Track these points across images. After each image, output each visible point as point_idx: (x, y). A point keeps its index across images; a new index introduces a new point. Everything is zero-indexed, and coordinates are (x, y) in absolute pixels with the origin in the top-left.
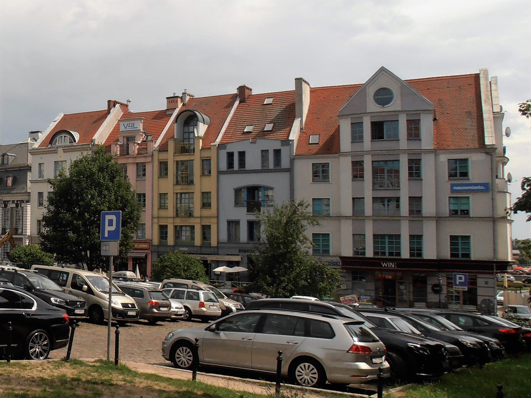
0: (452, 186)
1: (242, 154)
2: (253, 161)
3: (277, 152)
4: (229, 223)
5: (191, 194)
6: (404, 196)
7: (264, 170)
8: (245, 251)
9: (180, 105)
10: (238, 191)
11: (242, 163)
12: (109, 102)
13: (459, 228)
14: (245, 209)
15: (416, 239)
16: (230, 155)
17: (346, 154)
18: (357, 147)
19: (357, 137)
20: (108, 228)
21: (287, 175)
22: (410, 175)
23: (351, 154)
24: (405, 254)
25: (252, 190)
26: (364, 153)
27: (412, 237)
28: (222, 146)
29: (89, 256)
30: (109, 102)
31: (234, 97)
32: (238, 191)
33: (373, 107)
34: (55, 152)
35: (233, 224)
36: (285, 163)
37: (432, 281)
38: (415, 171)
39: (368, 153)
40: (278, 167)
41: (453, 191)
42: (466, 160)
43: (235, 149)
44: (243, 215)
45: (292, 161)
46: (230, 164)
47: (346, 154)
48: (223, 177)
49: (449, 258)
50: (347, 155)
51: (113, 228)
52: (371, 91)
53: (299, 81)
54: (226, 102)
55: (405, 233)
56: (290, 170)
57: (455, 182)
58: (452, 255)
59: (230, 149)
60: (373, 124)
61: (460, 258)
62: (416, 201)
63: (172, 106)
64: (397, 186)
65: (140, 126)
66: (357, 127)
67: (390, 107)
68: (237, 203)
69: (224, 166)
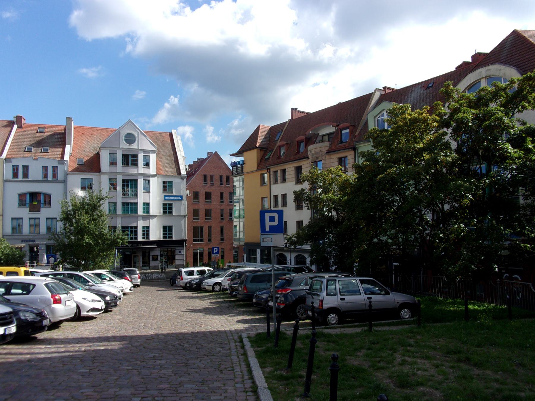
0: (165, 196)
1: (26, 168)
2: (35, 172)
3: (55, 168)
4: (144, 204)
5: (37, 221)
6: (141, 201)
8: (27, 241)
10: (22, 196)
11: (26, 175)
14: (28, 209)
15: (146, 230)
16: (15, 169)
17: (105, 173)
18: (113, 169)
19: (113, 163)
21: (61, 185)
23: (110, 174)
24: (140, 238)
25: (34, 196)
26: (116, 174)
27: (144, 204)
28: (7, 160)
29: (357, 133)
31: (11, 124)
32: (22, 196)
33: (124, 145)
36: (60, 176)
37: (152, 253)
38: (147, 190)
39: (119, 174)
41: (165, 199)
43: (20, 164)
44: (25, 213)
45: (66, 174)
46: (15, 175)
47: (105, 173)
48: (8, 184)
49: (162, 239)
50: (107, 174)
52: (123, 134)
53: (69, 119)
55: (141, 224)
56: (64, 182)
57: (167, 195)
58: (164, 237)
59: (15, 162)
60: (123, 155)
61: (167, 239)
62: (147, 206)
66: (112, 155)
67: (134, 146)
68: (22, 203)
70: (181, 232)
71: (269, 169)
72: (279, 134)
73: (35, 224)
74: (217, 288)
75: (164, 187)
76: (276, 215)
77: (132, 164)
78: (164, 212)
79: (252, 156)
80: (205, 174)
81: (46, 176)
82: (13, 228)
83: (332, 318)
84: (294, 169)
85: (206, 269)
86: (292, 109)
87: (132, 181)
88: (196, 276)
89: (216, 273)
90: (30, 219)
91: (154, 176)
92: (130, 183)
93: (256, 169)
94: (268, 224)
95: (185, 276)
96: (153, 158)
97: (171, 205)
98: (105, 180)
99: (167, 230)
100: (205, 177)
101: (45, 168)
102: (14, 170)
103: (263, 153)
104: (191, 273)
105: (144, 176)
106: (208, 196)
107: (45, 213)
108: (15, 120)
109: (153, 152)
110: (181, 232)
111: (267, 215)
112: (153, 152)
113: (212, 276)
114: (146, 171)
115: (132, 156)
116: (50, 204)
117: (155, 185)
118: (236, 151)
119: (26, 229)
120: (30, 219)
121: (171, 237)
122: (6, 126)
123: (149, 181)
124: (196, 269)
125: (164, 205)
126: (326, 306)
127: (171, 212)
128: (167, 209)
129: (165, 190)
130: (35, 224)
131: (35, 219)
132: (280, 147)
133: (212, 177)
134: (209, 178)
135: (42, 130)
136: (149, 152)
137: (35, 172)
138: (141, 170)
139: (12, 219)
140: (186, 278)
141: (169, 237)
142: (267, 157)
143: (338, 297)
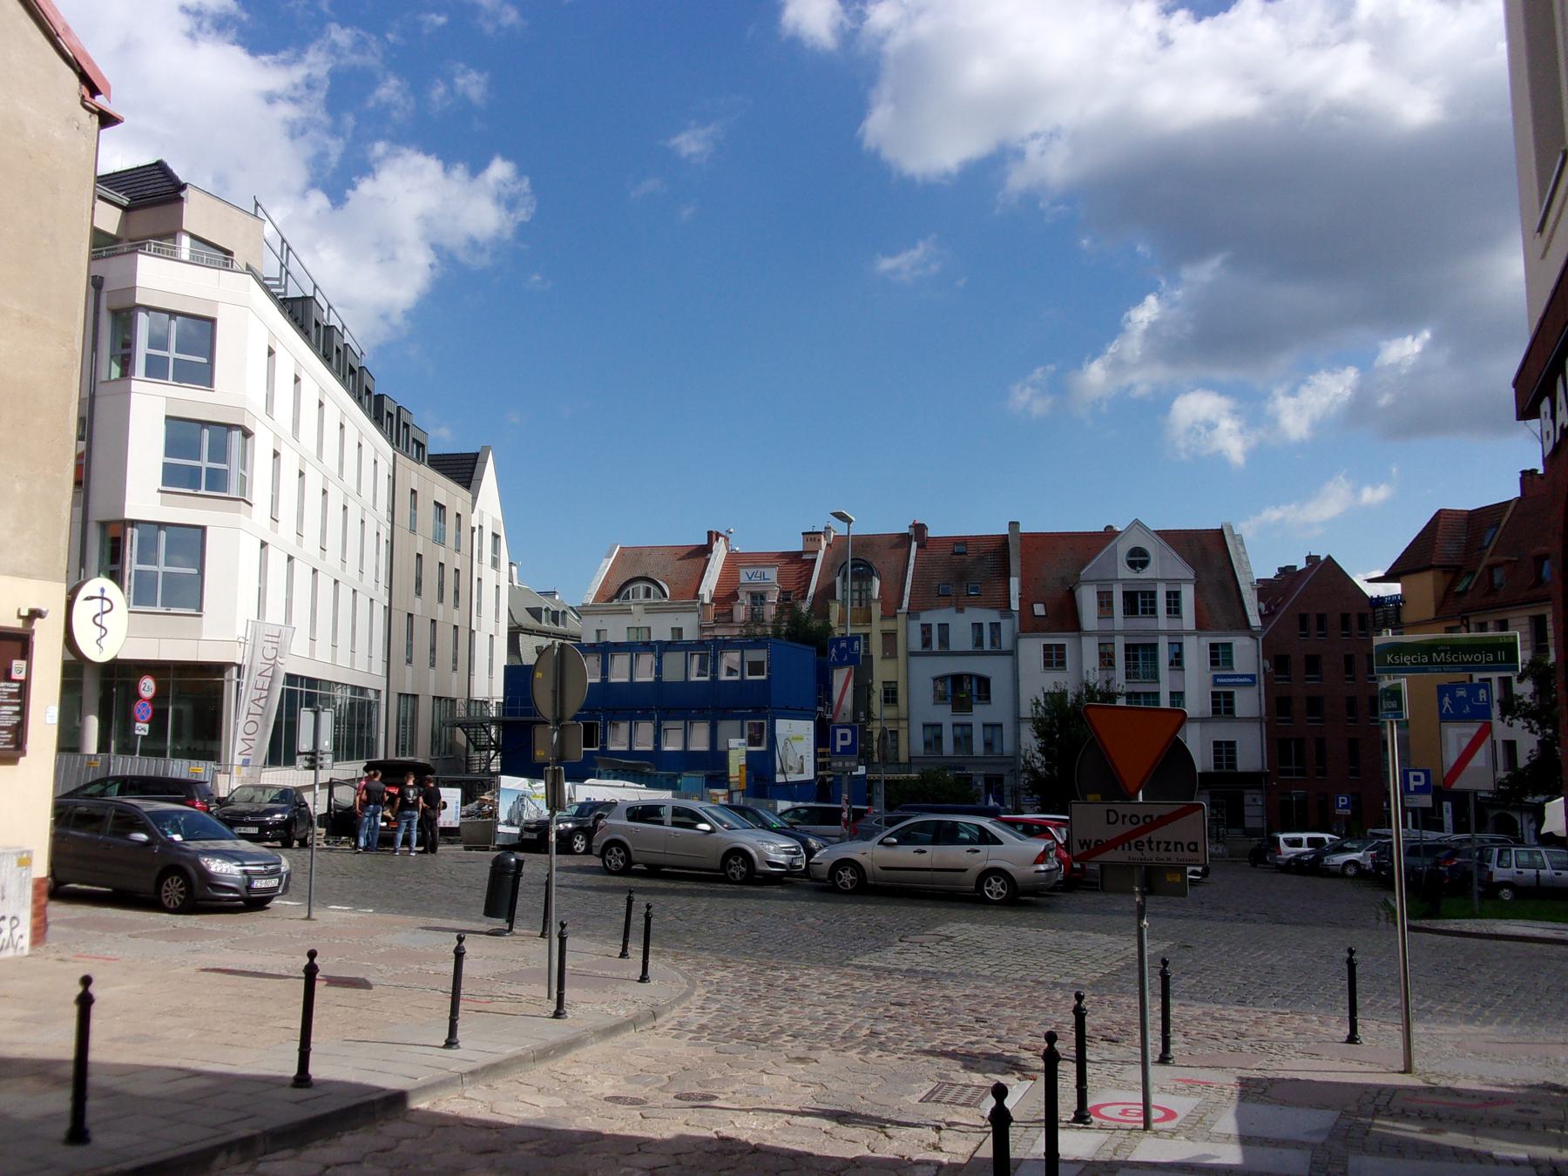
0: (1216, 677)
1: (944, 628)
2: (961, 637)
3: (995, 627)
4: (1505, 742)
7: (978, 651)
9: (824, 543)
11: (944, 640)
12: (710, 533)
13: (1223, 732)
17: (1090, 634)
20: (840, 743)
21: (1007, 660)
22: (1169, 611)
25: (957, 680)
26: (1112, 634)
27: (1172, 694)
30: (710, 533)
33: (1125, 572)
34: (628, 612)
35: (933, 730)
36: (1006, 643)
38: (1177, 662)
39: (1120, 633)
40: (997, 652)
41: (1216, 684)
42: (1229, 645)
44: (944, 715)
46: (927, 642)
47: (1090, 634)
48: (914, 659)
51: (848, 742)
54: (904, 540)
56: (1013, 653)
58: (1216, 766)
60: (1125, 594)
61: (1225, 769)
63: (811, 547)
64: (1154, 676)
65: (772, 574)
66: (1105, 601)
67: (1147, 573)
68: (940, 698)
69: (916, 644)
70: (1251, 755)
71: (1467, 618)
72: (1490, 534)
73: (963, 738)
74: (1351, 871)
75: (1212, 655)
76: (1422, 775)
77: (1144, 611)
78: (1216, 711)
79: (1427, 583)
80: (1303, 611)
81: (979, 641)
82: (927, 744)
83: (1506, 894)
84: (1526, 620)
85: (1326, 836)
86: (1523, 472)
87: (1145, 646)
88: (1305, 849)
89: (1348, 845)
90: (954, 725)
91: (1189, 633)
92: (1141, 655)
93: (1431, 614)
94: (1412, 784)
95: (1284, 848)
96: (1188, 595)
97: (1230, 695)
98: (1090, 648)
99: (1225, 751)
100: (1303, 619)
101: (978, 627)
102: (923, 633)
103: (1449, 577)
104: (1296, 843)
105: (1169, 633)
106: (1313, 663)
107: (980, 715)
108: (912, 532)
109: (1186, 581)
110: (1251, 755)
111: (1411, 774)
112: (1186, 581)
113: (1341, 850)
114: (1174, 624)
115: (1144, 594)
116: (988, 698)
117: (1196, 651)
118: (1381, 574)
119: (948, 747)
120: (954, 725)
121: (1234, 766)
122: (896, 546)
123: (1180, 645)
124: (1305, 836)
125: (1214, 694)
126: (1496, 878)
127: (1230, 711)
128: (1222, 705)
129: (1214, 663)
130: (963, 738)
131: (962, 725)
132: (1491, 568)
133: (1321, 619)
134: (1313, 623)
135: (962, 549)
136: (1178, 581)
137: (961, 637)
138: (1163, 621)
139: (925, 726)
140: (1287, 852)
141: (1229, 766)
142: (1460, 588)
143: (1514, 869)
